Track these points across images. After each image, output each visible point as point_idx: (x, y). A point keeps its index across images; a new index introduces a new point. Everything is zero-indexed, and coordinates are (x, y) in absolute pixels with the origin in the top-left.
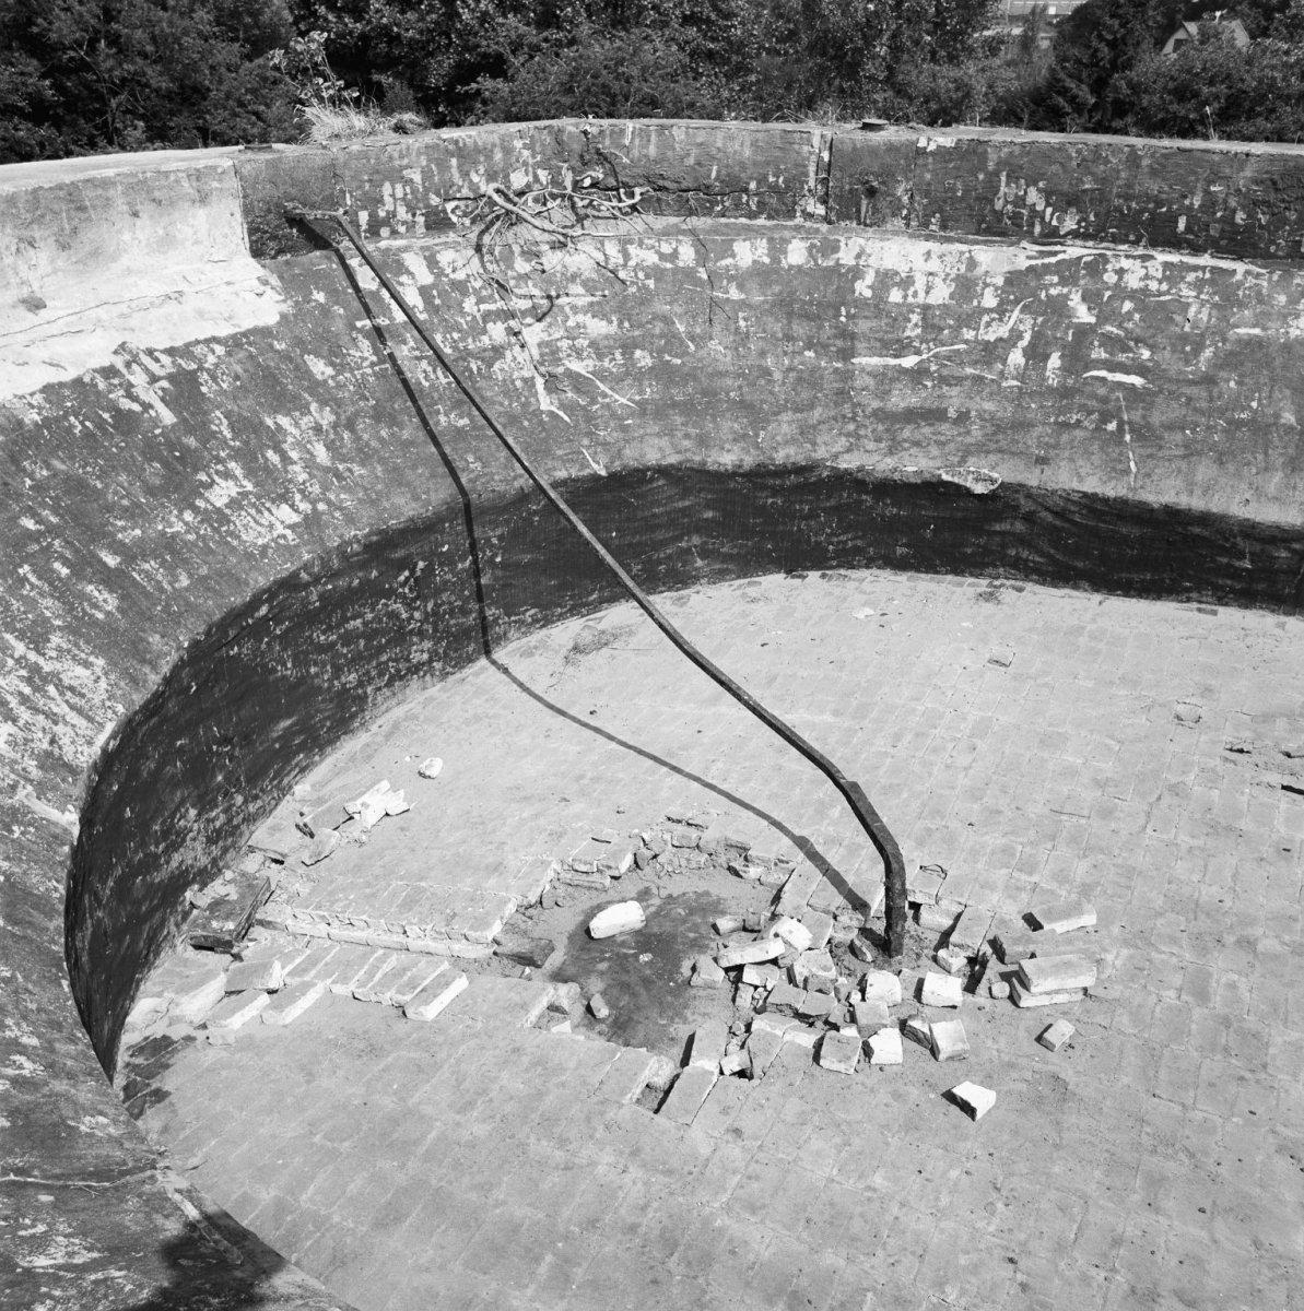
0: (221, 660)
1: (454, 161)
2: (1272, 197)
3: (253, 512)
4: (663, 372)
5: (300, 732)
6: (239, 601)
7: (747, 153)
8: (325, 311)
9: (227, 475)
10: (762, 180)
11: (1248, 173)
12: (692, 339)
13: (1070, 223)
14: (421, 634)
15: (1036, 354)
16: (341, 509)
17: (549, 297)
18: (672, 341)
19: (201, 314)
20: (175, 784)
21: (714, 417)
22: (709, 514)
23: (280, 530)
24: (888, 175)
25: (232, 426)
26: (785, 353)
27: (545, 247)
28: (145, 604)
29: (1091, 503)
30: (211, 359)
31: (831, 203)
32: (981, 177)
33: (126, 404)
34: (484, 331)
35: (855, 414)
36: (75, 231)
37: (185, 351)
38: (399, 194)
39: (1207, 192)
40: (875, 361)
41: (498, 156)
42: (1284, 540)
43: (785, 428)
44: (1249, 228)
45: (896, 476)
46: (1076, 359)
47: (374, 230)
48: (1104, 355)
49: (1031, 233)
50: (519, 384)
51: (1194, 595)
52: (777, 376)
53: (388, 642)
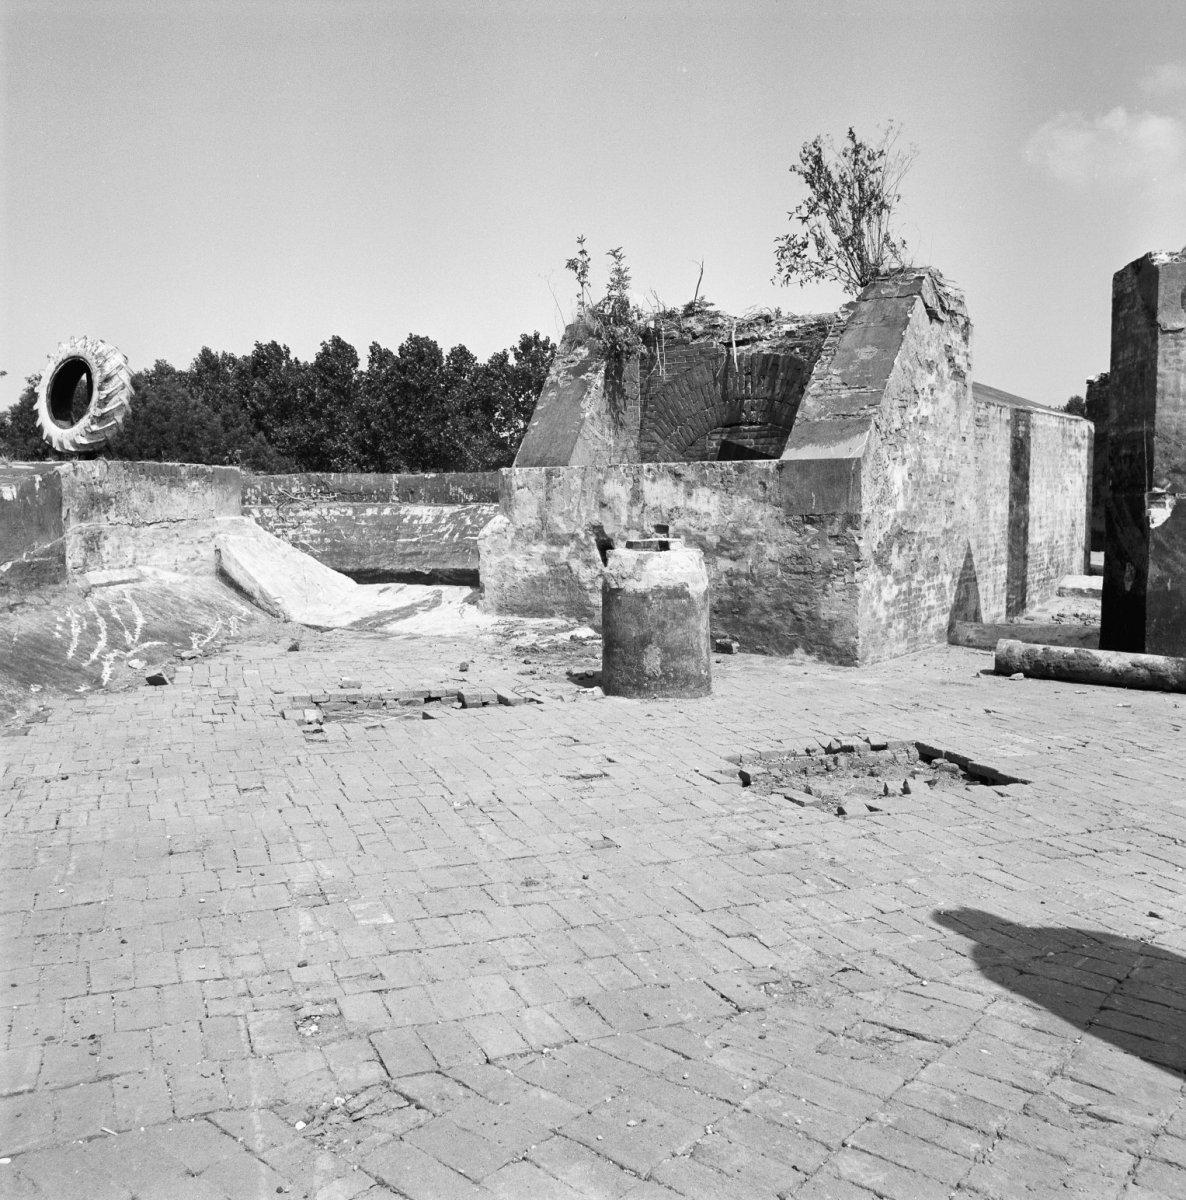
4: (333, 544)
18: (339, 536)
24: (416, 487)
40: (405, 540)
41: (288, 482)
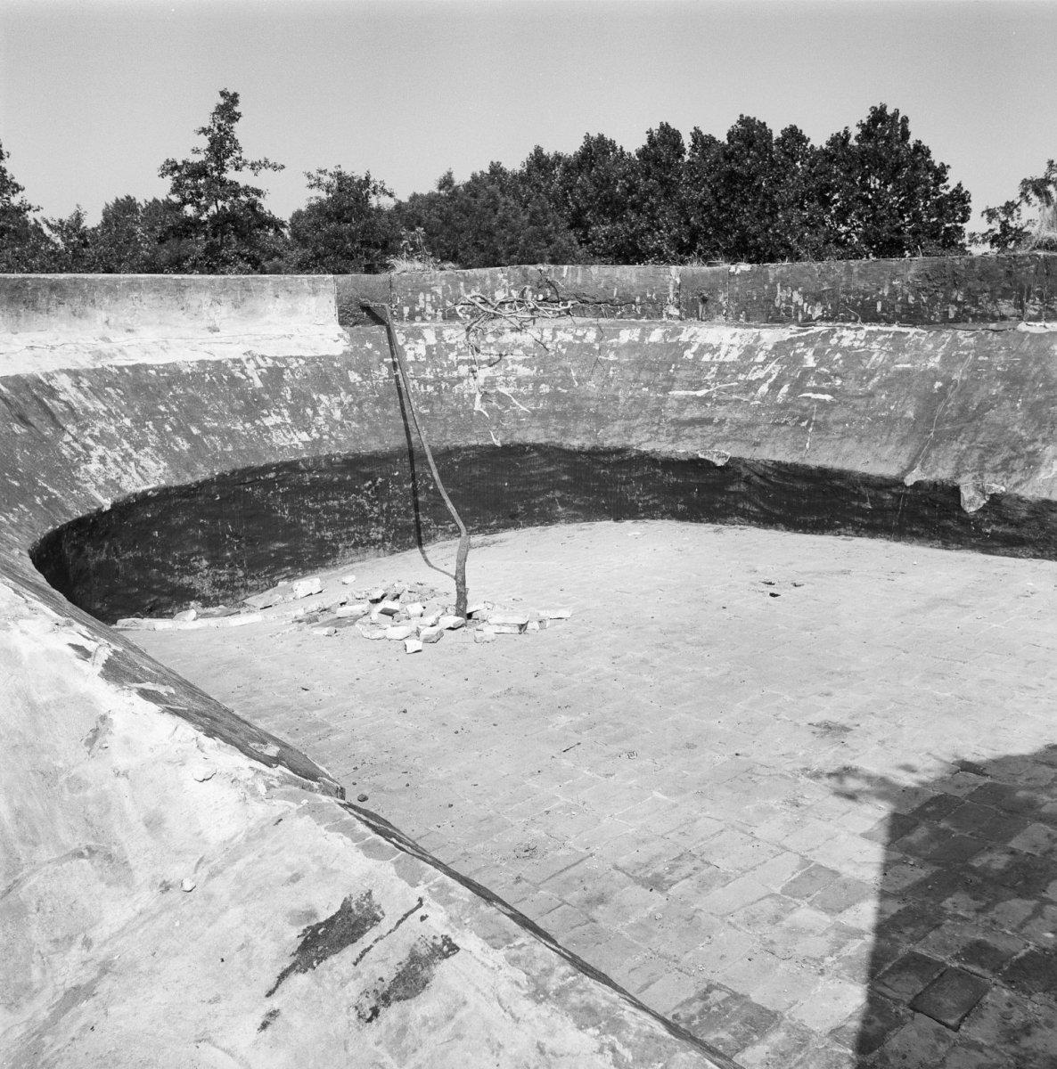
0: (239, 491)
1: (462, 284)
2: (927, 285)
3: (285, 431)
4: (554, 397)
5: (289, 554)
6: (256, 464)
7: (634, 280)
8: (369, 352)
9: (279, 414)
10: (643, 296)
11: (912, 271)
12: (578, 380)
13: (818, 312)
14: (378, 522)
15: (775, 387)
16: (336, 440)
17: (501, 355)
19: (299, 345)
20: (195, 540)
21: (576, 420)
22: (565, 478)
23: (296, 441)
24: (713, 290)
25: (292, 395)
26: (631, 389)
27: (507, 330)
28: (203, 451)
29: (780, 468)
30: (295, 365)
31: (682, 308)
32: (766, 287)
33: (238, 374)
34: (456, 369)
35: (660, 421)
36: (243, 300)
37: (283, 360)
38: (428, 298)
39: (891, 285)
40: (683, 393)
41: (488, 282)
42: (887, 487)
43: (617, 428)
44: (917, 306)
45: (673, 456)
46: (798, 386)
47: (412, 317)
48: (814, 384)
49: (797, 320)
50: (466, 396)
51: (842, 530)
52: (622, 401)
53: (356, 521)
